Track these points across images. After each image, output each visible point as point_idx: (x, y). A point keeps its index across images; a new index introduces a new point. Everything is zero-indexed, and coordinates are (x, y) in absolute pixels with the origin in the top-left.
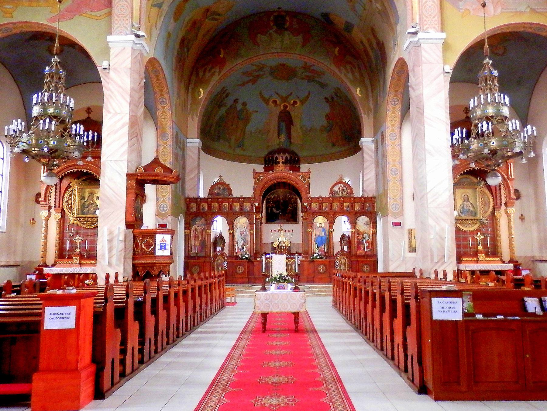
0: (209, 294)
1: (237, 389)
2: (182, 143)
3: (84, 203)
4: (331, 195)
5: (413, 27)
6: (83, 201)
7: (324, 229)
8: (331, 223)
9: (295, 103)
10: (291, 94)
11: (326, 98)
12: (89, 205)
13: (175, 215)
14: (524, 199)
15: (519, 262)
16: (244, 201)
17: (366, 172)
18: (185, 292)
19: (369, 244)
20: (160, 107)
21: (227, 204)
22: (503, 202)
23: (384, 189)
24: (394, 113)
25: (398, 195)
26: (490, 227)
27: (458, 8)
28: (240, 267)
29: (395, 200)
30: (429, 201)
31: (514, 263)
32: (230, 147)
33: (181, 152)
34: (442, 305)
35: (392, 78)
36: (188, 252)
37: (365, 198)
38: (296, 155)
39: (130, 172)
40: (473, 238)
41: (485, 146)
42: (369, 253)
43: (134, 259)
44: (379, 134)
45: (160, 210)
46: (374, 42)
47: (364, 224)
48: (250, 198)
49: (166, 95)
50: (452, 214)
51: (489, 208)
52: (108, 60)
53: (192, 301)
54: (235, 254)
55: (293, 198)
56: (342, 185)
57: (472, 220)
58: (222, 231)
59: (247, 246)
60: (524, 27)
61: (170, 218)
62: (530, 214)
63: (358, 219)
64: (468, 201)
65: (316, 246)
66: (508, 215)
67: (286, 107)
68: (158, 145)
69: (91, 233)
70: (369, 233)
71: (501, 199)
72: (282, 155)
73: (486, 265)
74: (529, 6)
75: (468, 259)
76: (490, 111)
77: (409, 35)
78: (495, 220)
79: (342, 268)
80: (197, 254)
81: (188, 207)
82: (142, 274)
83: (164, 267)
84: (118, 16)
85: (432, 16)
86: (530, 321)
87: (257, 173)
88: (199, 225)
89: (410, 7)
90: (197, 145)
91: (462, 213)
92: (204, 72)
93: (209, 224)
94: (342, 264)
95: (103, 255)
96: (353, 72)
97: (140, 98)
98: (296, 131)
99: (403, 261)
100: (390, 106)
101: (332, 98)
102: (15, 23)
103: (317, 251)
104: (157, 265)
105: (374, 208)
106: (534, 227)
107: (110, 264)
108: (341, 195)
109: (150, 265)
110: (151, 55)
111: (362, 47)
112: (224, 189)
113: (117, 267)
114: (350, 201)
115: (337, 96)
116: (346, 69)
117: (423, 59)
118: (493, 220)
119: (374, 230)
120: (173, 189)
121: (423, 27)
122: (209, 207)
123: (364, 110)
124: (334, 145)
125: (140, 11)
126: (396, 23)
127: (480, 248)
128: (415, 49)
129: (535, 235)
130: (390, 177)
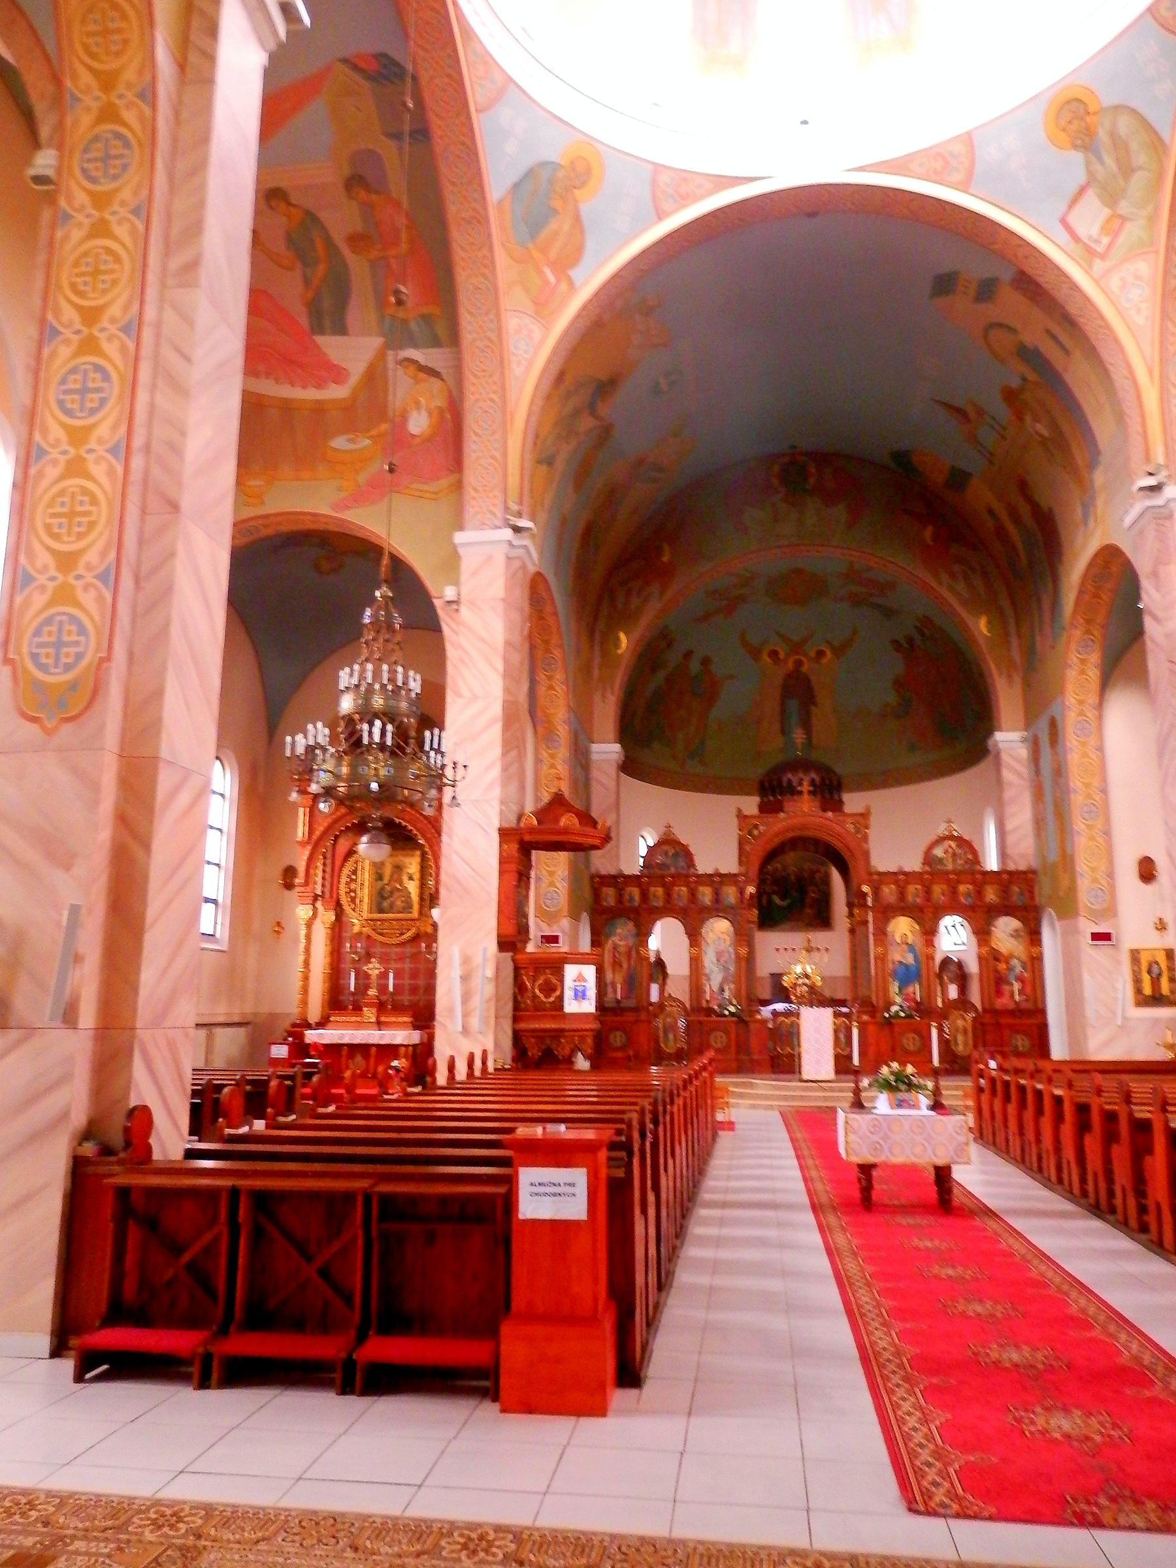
3: (382, 889)
4: (927, 868)
5: (1151, 474)
6: (380, 884)
7: (911, 948)
9: (820, 654)
10: (855, 632)
11: (896, 645)
12: (392, 893)
13: (575, 916)
16: (721, 883)
17: (1010, 810)
28: (718, 1034)
32: (674, 757)
35: (1081, 592)
37: (1010, 873)
39: (506, 825)
42: (1025, 1006)
43: (516, 1019)
46: (1025, 511)
49: (555, 652)
52: (456, 583)
55: (818, 871)
58: (660, 949)
61: (565, 923)
67: (799, 663)
69: (396, 953)
70: (1024, 957)
77: (1142, 493)
80: (618, 1002)
81: (597, 895)
82: (534, 1052)
84: (476, 490)
87: (746, 817)
88: (621, 934)
89: (1139, 428)
92: (629, 593)
93: (643, 934)
95: (451, 1010)
96: (966, 578)
98: (822, 715)
100: (1074, 658)
101: (910, 640)
102: (267, 516)
103: (898, 1000)
105: (1032, 898)
107: (466, 1031)
109: (552, 1034)
111: (990, 523)
112: (676, 855)
113: (480, 1037)
114: (973, 883)
115: (923, 635)
116: (953, 576)
119: (1034, 950)
122: (645, 896)
123: (996, 665)
126: (1092, 465)
128: (1158, 524)
130: (1079, 825)
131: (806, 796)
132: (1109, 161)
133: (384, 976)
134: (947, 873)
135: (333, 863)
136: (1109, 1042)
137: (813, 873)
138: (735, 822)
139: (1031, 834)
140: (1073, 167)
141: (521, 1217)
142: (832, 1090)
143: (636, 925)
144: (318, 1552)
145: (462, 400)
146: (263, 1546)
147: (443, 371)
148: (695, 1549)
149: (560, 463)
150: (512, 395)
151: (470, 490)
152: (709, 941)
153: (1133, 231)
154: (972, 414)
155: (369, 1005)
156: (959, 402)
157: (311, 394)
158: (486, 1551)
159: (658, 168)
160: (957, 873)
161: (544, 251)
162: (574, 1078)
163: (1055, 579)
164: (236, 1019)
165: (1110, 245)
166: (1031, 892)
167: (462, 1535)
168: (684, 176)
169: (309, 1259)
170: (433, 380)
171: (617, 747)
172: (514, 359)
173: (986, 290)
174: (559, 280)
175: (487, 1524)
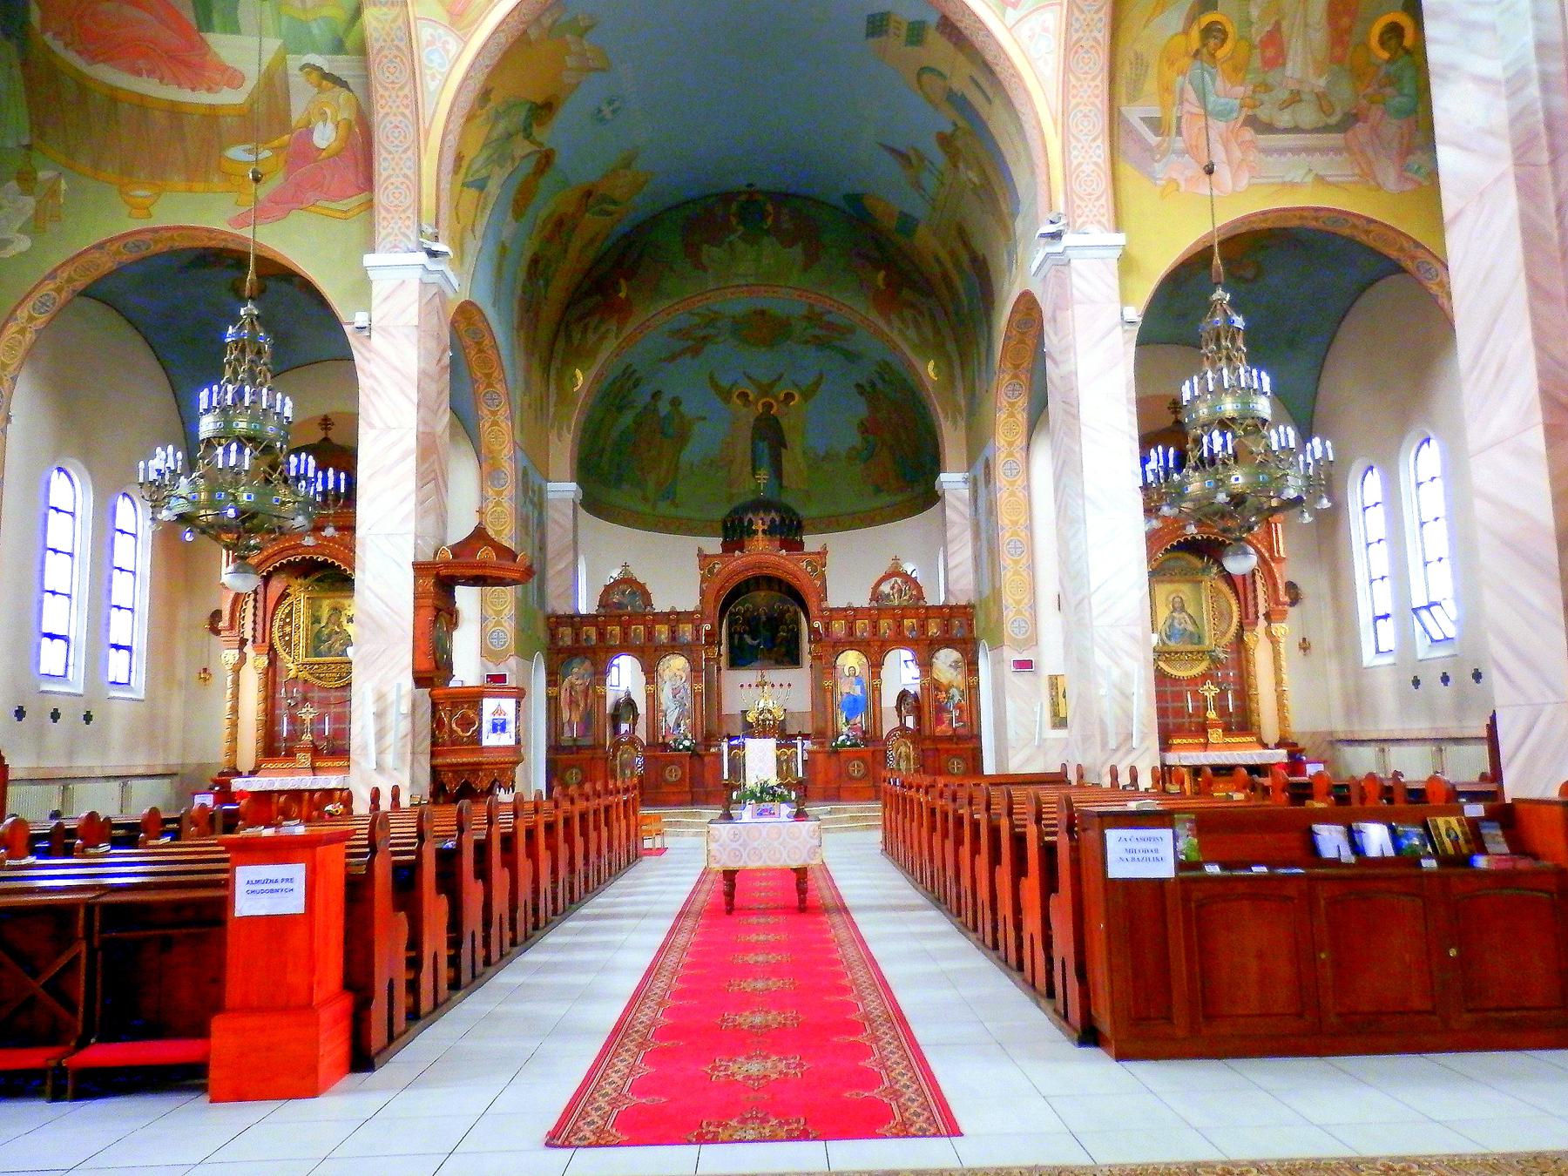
3: (320, 631)
4: (874, 604)
5: (1052, 222)
6: (317, 627)
7: (859, 681)
8: (876, 666)
9: (789, 397)
11: (858, 386)
12: (330, 636)
13: (525, 654)
14: (1308, 602)
16: (678, 621)
17: (952, 548)
19: (961, 711)
20: (486, 412)
21: (642, 627)
22: (1262, 610)
24: (1012, 415)
25: (1026, 600)
26: (1233, 668)
27: (1152, 177)
29: (1019, 612)
30: (1095, 613)
32: (645, 499)
33: (536, 514)
34: (1129, 845)
35: (1007, 337)
37: (951, 608)
38: (794, 514)
39: (421, 559)
41: (1217, 487)
42: (962, 731)
43: (433, 755)
46: (965, 257)
48: (693, 613)
49: (498, 386)
50: (1147, 640)
51: (1230, 626)
52: (368, 310)
55: (788, 611)
56: (899, 581)
57: (1191, 652)
60: (1301, 218)
61: (513, 662)
62: (1324, 637)
63: (937, 655)
64: (1182, 609)
65: (842, 719)
66: (1274, 641)
67: (769, 406)
69: (335, 697)
71: (1256, 605)
73: (1227, 753)
74: (1310, 170)
75: (1185, 741)
76: (1229, 407)
77: (1043, 240)
78: (1243, 652)
80: (575, 740)
81: (553, 636)
82: (452, 787)
85: (1093, 197)
86: (1326, 878)
88: (578, 675)
89: (1044, 178)
90: (572, 495)
91: (1169, 637)
94: (902, 757)
95: (365, 748)
96: (918, 326)
97: (440, 393)
98: (793, 461)
99: (1039, 747)
100: (1003, 401)
102: (155, 230)
103: (845, 729)
105: (972, 631)
106: (1333, 667)
107: (380, 767)
109: (470, 767)
110: (465, 297)
112: (633, 593)
113: (395, 773)
114: (917, 616)
115: (884, 380)
116: (903, 320)
117: (1075, 291)
118: (1239, 652)
121: (1075, 222)
122: (602, 635)
123: (944, 410)
124: (878, 490)
126: (1014, 216)
127: (1212, 715)
128: (1057, 271)
129: (1335, 684)
130: (1006, 560)
133: (321, 719)
134: (894, 609)
135: (265, 607)
136: (1028, 761)
137: (782, 613)
139: (971, 570)
141: (237, 914)
145: (371, 113)
147: (350, 81)
149: (493, 187)
150: (426, 113)
151: (382, 211)
154: (914, 159)
155: (304, 750)
156: (899, 145)
157: (203, 98)
160: (903, 608)
163: (990, 328)
164: (159, 771)
166: (971, 625)
169: (35, 973)
170: (338, 89)
171: (573, 486)
172: (428, 72)
173: (916, 34)
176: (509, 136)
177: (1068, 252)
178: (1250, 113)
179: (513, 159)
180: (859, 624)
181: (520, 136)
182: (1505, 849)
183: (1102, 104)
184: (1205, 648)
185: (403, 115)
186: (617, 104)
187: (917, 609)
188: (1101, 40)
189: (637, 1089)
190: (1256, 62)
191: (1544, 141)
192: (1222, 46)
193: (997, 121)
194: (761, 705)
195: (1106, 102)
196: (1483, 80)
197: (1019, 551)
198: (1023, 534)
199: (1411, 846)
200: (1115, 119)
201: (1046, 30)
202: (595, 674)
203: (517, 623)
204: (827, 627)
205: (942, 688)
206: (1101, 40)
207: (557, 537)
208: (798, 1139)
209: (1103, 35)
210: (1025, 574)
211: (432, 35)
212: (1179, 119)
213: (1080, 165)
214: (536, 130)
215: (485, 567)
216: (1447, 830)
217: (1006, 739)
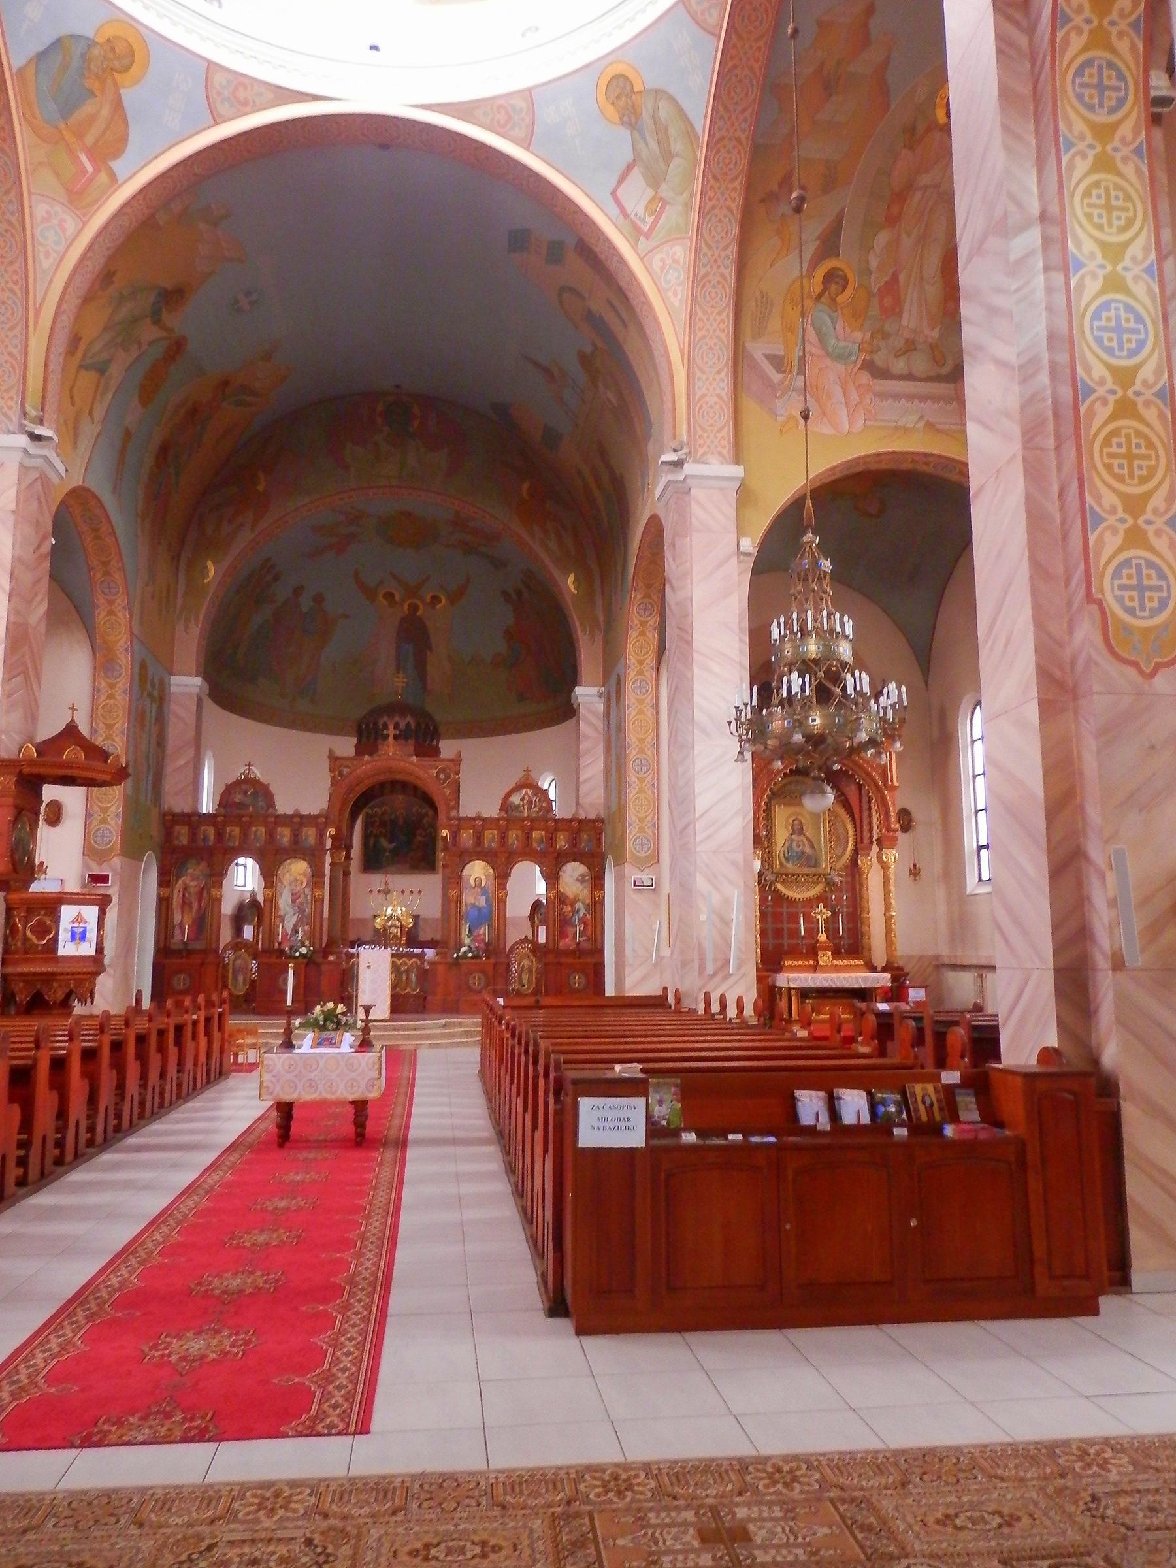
0: (173, 1050)
1: (126, 1312)
2: (157, 686)
4: (503, 814)
5: (675, 450)
7: (484, 891)
8: (502, 877)
9: (435, 599)
10: (428, 578)
11: (505, 593)
14: (919, 829)
15: (905, 970)
16: (301, 824)
17: (583, 762)
18: (141, 1039)
20: (102, 601)
21: (263, 830)
22: (875, 837)
23: (619, 803)
24: (642, 633)
25: (649, 818)
27: (773, 412)
29: (642, 830)
30: (698, 839)
31: (894, 972)
33: (155, 707)
34: (601, 1114)
36: (166, 938)
37: (580, 821)
38: (431, 718)
40: (808, 919)
41: (795, 727)
42: (586, 946)
44: (613, 681)
45: (95, 841)
46: (605, 477)
47: (577, 880)
48: (316, 817)
50: (748, 865)
51: (845, 849)
53: (138, 1062)
54: (276, 946)
55: (426, 815)
56: (530, 793)
59: (306, 928)
60: (913, 461)
61: (117, 862)
62: (933, 866)
65: (465, 930)
66: (885, 867)
67: (414, 608)
68: (95, 690)
71: (871, 830)
72: (397, 719)
74: (921, 417)
75: (795, 963)
76: (812, 648)
77: (666, 468)
78: (857, 876)
79: (525, 978)
80: (185, 944)
81: (168, 833)
83: (79, 982)
86: (798, 1148)
87: (337, 759)
88: (191, 877)
89: (670, 405)
90: (196, 690)
91: (787, 860)
93: (217, 875)
94: (524, 971)
97: (37, 582)
98: (438, 665)
99: (656, 965)
100: (635, 619)
101: (519, 593)
103: (467, 941)
104: (62, 977)
105: (599, 846)
106: (941, 893)
108: (526, 814)
110: (76, 481)
112: (255, 794)
114: (546, 829)
117: (693, 520)
118: (853, 876)
120: (130, 791)
121: (696, 451)
122: (219, 835)
124: (521, 698)
125: (45, 380)
127: (822, 937)
129: (942, 908)
130: (631, 777)
131: (391, 739)
132: (653, 144)
134: (524, 820)
136: (645, 978)
138: (326, 764)
140: (621, 145)
142: (386, 1029)
143: (210, 865)
144: (96, 1534)
146: (30, 1536)
148: (496, 1478)
149: (116, 372)
152: (285, 882)
153: (672, 216)
158: (285, 1507)
159: (211, 66)
161: (80, 136)
162: (16, 1024)
165: (655, 222)
167: (255, 1496)
168: (241, 81)
171: (197, 681)
173: (555, 253)
174: (97, 170)
175: (280, 1481)
176: (135, 320)
177: (688, 480)
178: (868, 358)
179: (140, 344)
180: (488, 834)
181: (148, 320)
182: (975, 1116)
183: (727, 337)
184: (820, 871)
185: (12, 291)
186: (254, 297)
187: (547, 821)
188: (728, 276)
189: (51, 1379)
190: (874, 310)
191: (1051, 427)
192: (842, 293)
193: (631, 346)
194: (389, 912)
195: (731, 337)
196: (1002, 364)
197: (645, 769)
198: (649, 753)
199: (887, 1112)
200: (739, 358)
201: (676, 261)
202: (211, 875)
203: (124, 820)
204: (455, 835)
205: (567, 901)
206: (728, 276)
207: (178, 729)
208: (191, 1440)
209: (729, 272)
210: (649, 792)
211: (48, 212)
212: (802, 358)
213: (703, 396)
214: (165, 316)
215: (71, 767)
216: (923, 1097)
217: (624, 956)
